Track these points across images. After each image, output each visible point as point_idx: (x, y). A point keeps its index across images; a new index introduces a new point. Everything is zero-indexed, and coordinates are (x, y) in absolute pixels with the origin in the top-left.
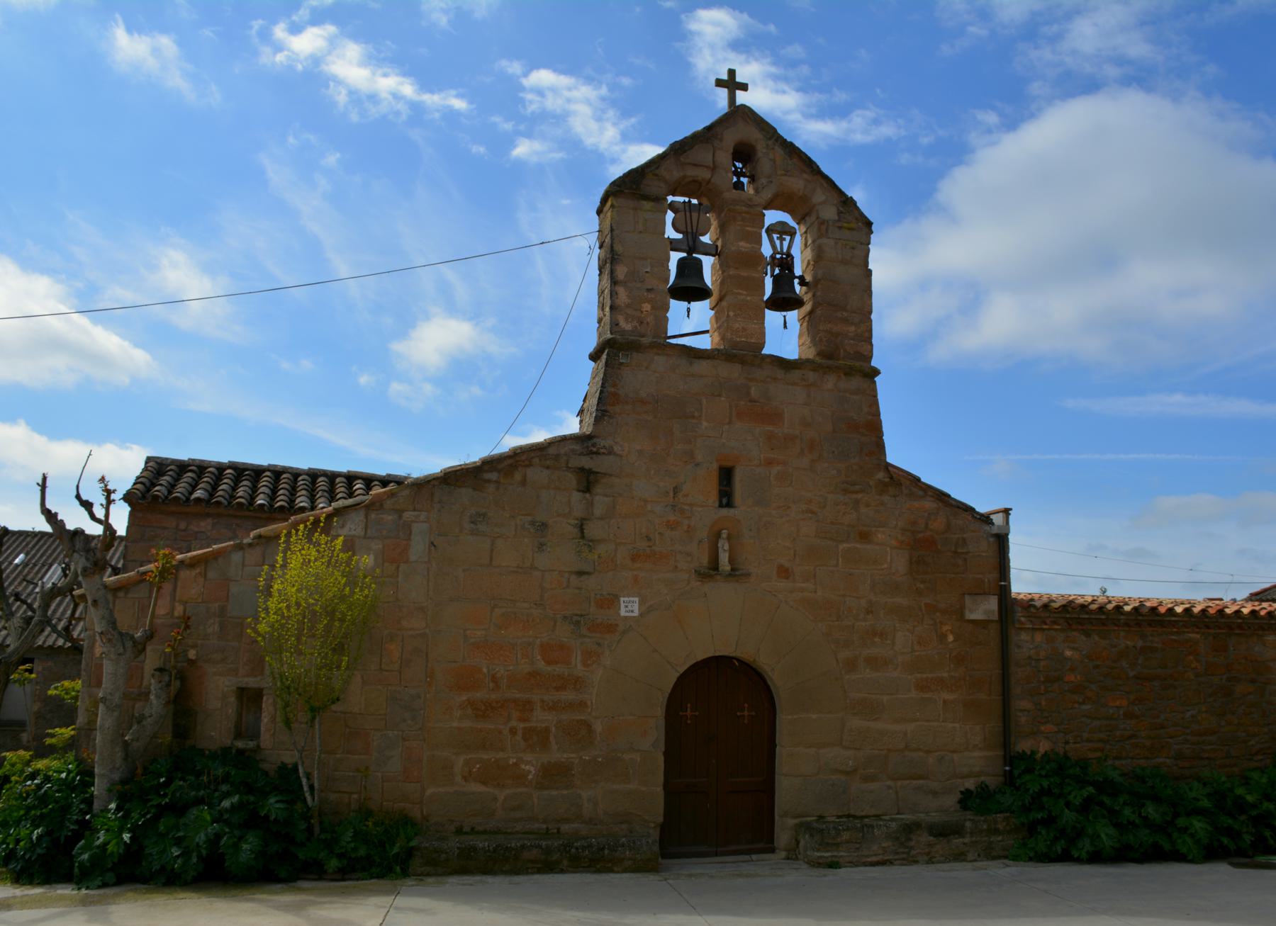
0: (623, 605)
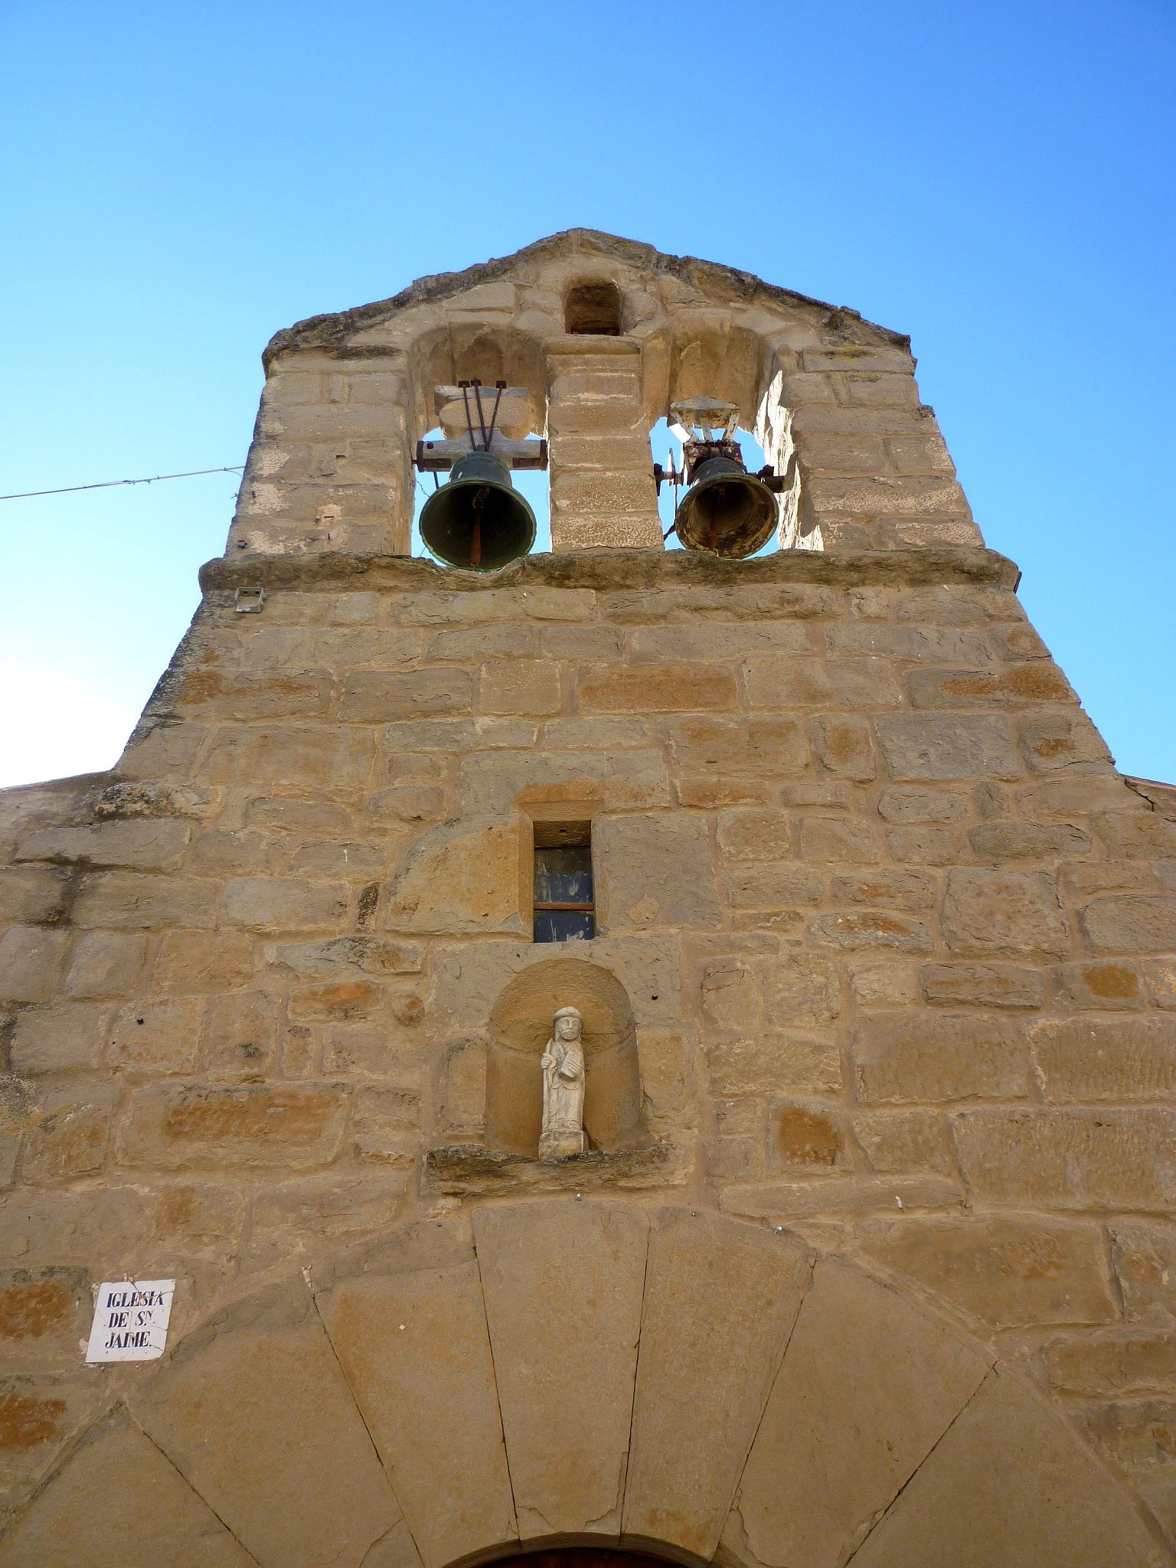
0: (102, 1313)
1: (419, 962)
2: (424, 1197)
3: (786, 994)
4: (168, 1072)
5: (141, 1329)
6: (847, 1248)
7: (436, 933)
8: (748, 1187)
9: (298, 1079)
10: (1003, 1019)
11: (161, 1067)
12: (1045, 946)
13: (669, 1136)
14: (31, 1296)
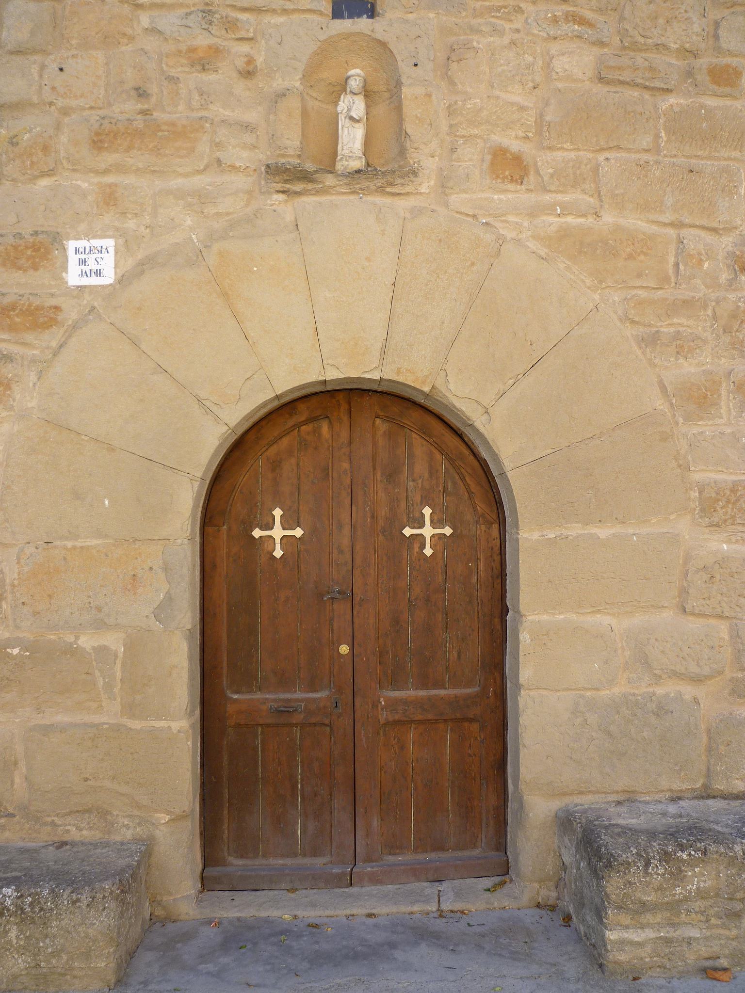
0: (73, 259)
1: (252, 30)
2: (264, 193)
3: (505, 68)
4: (87, 106)
5: (98, 267)
6: (523, 236)
7: (264, 9)
8: (467, 196)
9: (175, 113)
10: (647, 96)
11: (81, 102)
12: (687, 46)
13: (419, 161)
14: (27, 248)
